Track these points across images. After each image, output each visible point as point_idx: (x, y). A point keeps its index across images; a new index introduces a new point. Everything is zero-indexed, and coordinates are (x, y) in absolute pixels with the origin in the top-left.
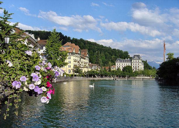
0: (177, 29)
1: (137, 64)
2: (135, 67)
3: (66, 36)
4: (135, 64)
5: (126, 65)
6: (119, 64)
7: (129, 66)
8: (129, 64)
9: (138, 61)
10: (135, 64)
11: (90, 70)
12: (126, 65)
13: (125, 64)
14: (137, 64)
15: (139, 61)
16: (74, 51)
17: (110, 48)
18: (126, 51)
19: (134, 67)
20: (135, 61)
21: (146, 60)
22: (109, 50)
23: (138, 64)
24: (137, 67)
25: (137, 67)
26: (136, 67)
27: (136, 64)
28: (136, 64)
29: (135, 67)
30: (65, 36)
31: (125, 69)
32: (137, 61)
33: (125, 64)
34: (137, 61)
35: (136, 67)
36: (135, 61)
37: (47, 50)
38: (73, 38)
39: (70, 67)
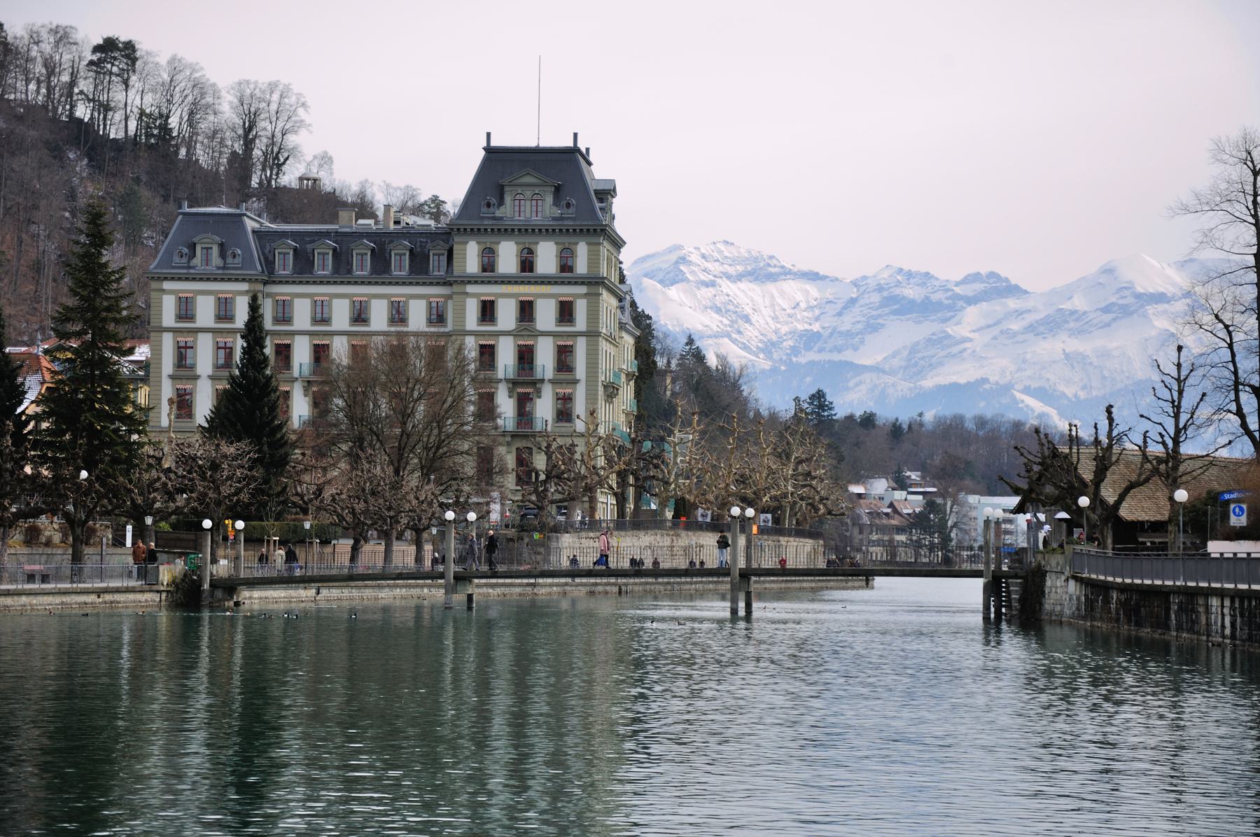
1: (546, 316)
4: (507, 315)
5: (379, 318)
8: (398, 315)
9: (527, 264)
10: (507, 315)
11: (807, 327)
12: (379, 318)
13: (360, 316)
14: (546, 316)
15: (582, 250)
20: (508, 256)
23: (566, 312)
26: (525, 356)
27: (526, 310)
28: (526, 310)
31: (68, 339)
32: (547, 257)
33: (360, 316)
34: (547, 257)
35: (525, 356)
36: (508, 256)
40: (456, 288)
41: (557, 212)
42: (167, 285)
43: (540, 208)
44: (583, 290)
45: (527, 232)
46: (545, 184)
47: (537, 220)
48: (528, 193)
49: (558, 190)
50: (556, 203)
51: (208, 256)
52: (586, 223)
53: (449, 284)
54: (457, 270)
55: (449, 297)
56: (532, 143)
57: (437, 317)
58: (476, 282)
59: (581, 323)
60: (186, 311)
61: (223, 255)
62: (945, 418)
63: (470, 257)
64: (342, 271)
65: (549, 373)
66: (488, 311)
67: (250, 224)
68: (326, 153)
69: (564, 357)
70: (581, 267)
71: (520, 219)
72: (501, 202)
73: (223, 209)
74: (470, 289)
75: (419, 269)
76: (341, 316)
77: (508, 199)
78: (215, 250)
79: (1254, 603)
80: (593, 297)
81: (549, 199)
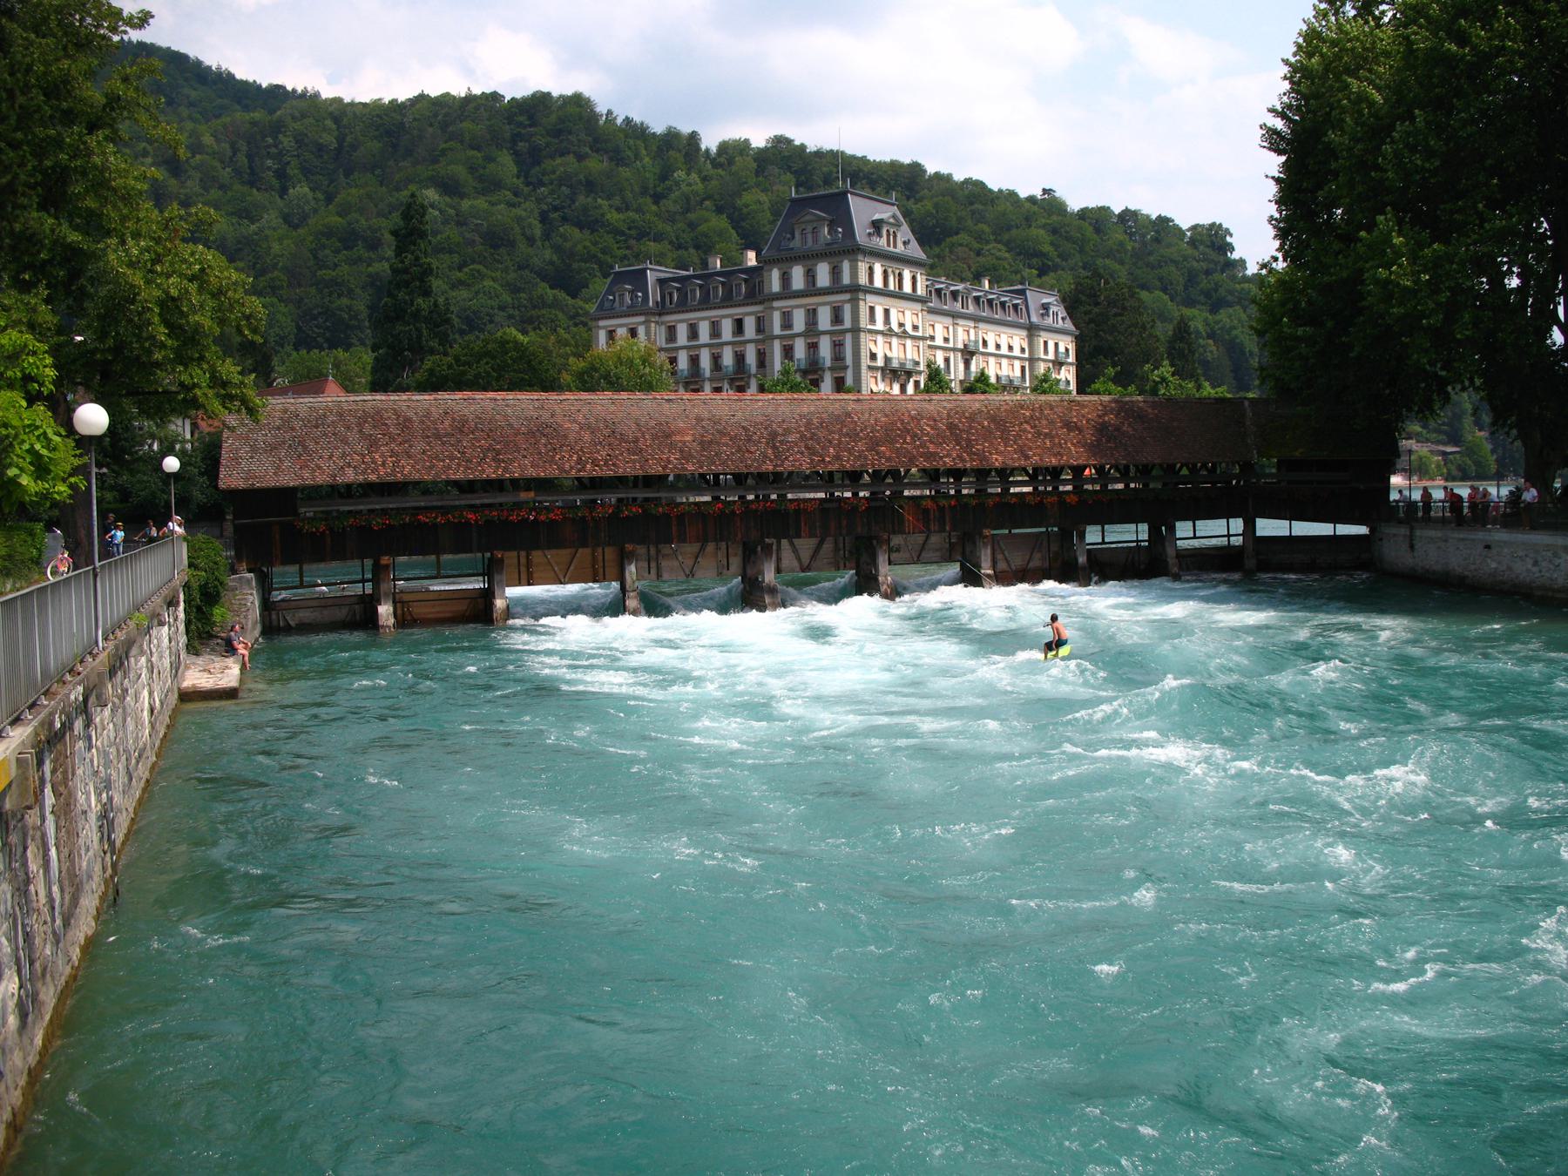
1: (824, 320)
2: (728, 359)
14: (824, 320)
15: (846, 266)
17: (1049, 204)
19: (788, 352)
23: (837, 318)
26: (694, 361)
27: (812, 315)
28: (812, 315)
35: (694, 361)
40: (766, 304)
44: (847, 296)
53: (761, 303)
58: (777, 299)
59: (848, 324)
60: (787, 323)
65: (828, 363)
68: (627, 118)
74: (776, 304)
80: (855, 302)
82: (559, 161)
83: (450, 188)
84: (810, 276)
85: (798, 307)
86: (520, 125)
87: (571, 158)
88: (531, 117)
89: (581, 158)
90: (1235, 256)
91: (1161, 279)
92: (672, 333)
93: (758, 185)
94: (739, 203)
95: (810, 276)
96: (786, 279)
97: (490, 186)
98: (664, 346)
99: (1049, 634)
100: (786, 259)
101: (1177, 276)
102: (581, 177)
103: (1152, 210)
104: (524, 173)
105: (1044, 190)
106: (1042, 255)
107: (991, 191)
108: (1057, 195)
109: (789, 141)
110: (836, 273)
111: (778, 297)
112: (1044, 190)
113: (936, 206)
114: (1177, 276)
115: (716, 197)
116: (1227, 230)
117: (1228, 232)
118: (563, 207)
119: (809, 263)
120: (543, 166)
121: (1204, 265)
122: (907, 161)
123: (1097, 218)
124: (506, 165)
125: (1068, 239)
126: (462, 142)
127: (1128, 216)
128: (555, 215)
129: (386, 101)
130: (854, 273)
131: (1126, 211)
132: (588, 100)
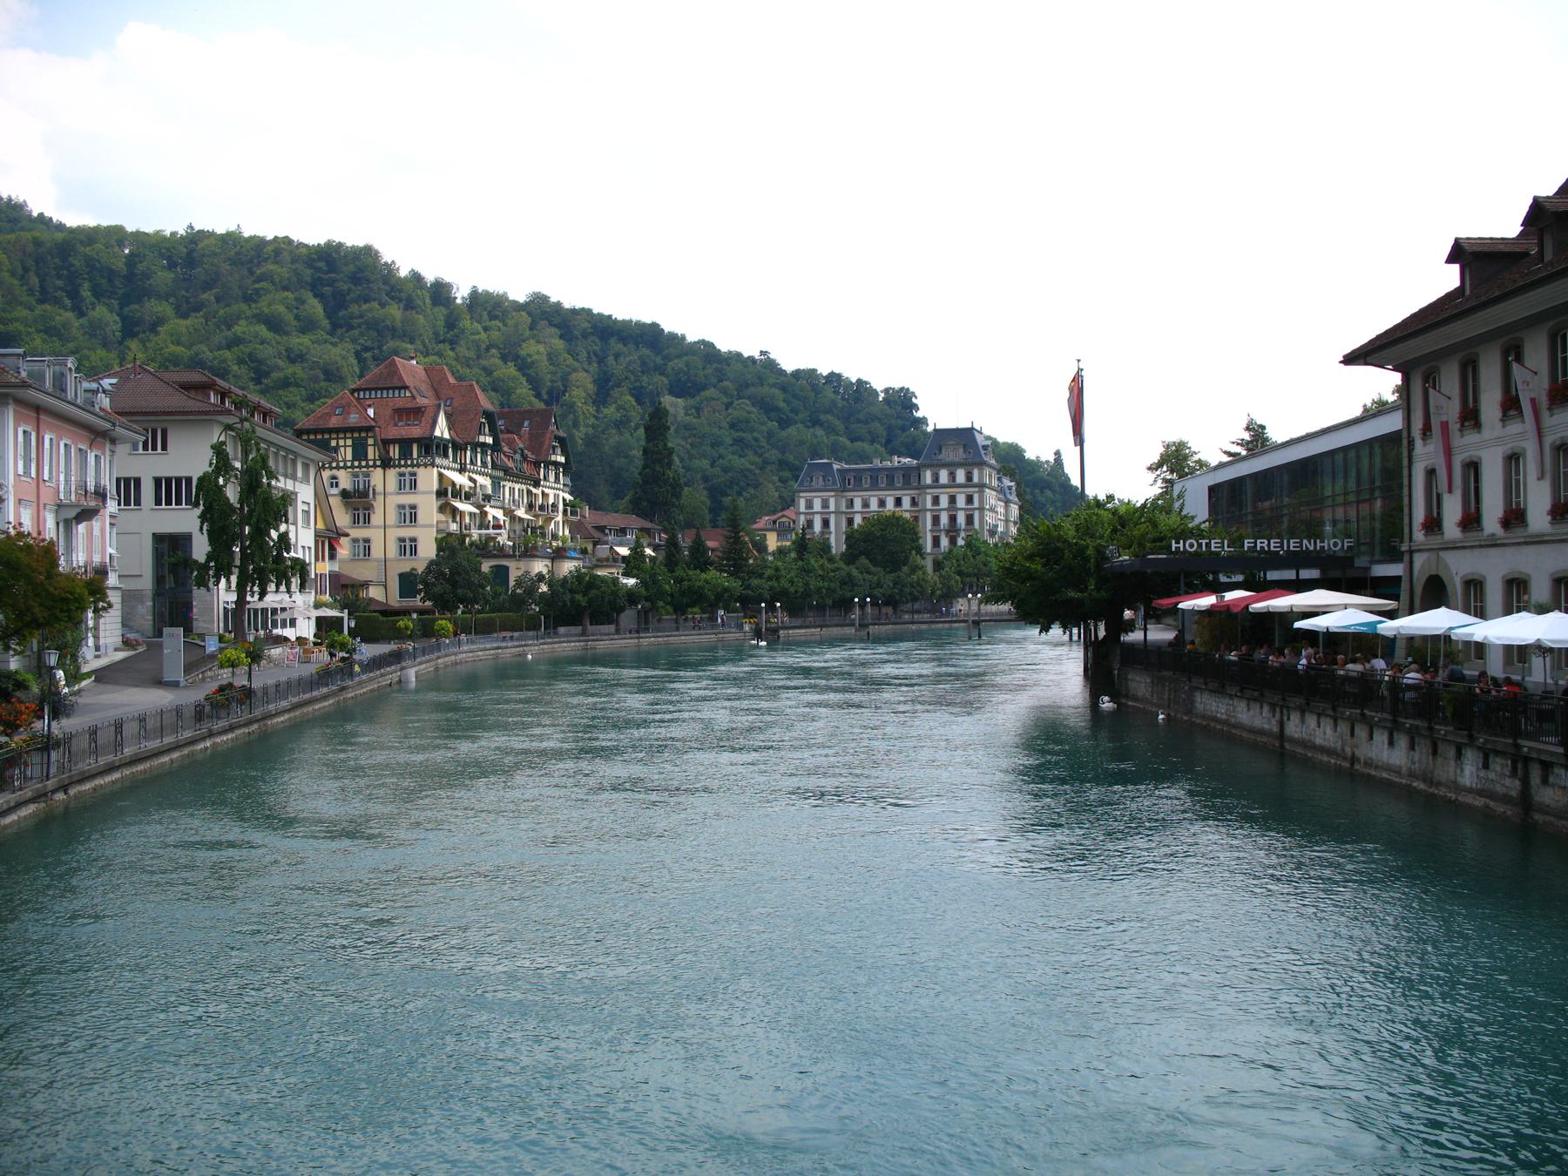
0: (605, 666)
1: (961, 501)
2: (944, 519)
3: (416, 278)
5: (874, 505)
6: (825, 504)
7: (893, 521)
12: (874, 505)
13: (866, 504)
14: (961, 501)
15: (976, 473)
16: (442, 430)
17: (767, 367)
18: (897, 385)
19: (936, 520)
20: (944, 476)
21: (1058, 453)
22: (761, 381)
23: (970, 499)
24: (961, 519)
25: (961, 519)
26: (953, 519)
27: (952, 499)
28: (952, 499)
29: (944, 519)
30: (403, 273)
32: (961, 476)
33: (866, 504)
34: (961, 476)
35: (953, 519)
37: (12, 635)
38: (475, 295)
39: (414, 551)
41: (964, 456)
42: (801, 494)
43: (960, 455)
44: (977, 489)
45: (952, 466)
46: (958, 444)
47: (957, 460)
48: (952, 448)
49: (965, 446)
50: (965, 452)
51: (819, 481)
52: (977, 460)
54: (922, 483)
55: (919, 494)
56: (954, 427)
57: (914, 502)
59: (976, 504)
60: (809, 505)
61: (824, 480)
62: (631, 321)
63: (928, 477)
64: (874, 486)
65: (963, 527)
66: (936, 500)
67: (836, 467)
68: (412, 270)
69: (970, 519)
70: (976, 479)
71: (948, 460)
72: (940, 452)
73: (825, 461)
74: (928, 491)
75: (907, 484)
76: (858, 505)
77: (943, 451)
78: (821, 479)
79: (1358, 655)
80: (981, 493)
81: (961, 450)
82: (365, 307)
83: (274, 324)
84: (952, 476)
85: (960, 493)
86: (318, 270)
87: (375, 305)
88: (328, 264)
89: (383, 305)
90: (919, 414)
91: (869, 432)
92: (851, 503)
93: (533, 337)
94: (523, 353)
95: (952, 476)
96: (936, 478)
97: (308, 326)
98: (844, 510)
99: (1054, 1087)
100: (936, 466)
101: (880, 430)
102: (388, 323)
103: (852, 374)
104: (330, 314)
105: (761, 352)
106: (778, 409)
107: (782, 372)
108: (771, 356)
109: (545, 299)
110: (969, 477)
111: (929, 487)
112: (761, 352)
113: (687, 364)
114: (880, 430)
115: (501, 346)
116: (913, 393)
117: (913, 395)
118: (373, 348)
119: (952, 469)
120: (350, 310)
121: (900, 422)
122: (648, 321)
123: (807, 377)
124: (315, 307)
125: (795, 396)
126: (273, 283)
127: (834, 378)
128: (368, 355)
129: (168, 233)
130: (981, 477)
131: (832, 374)
132: (377, 252)
